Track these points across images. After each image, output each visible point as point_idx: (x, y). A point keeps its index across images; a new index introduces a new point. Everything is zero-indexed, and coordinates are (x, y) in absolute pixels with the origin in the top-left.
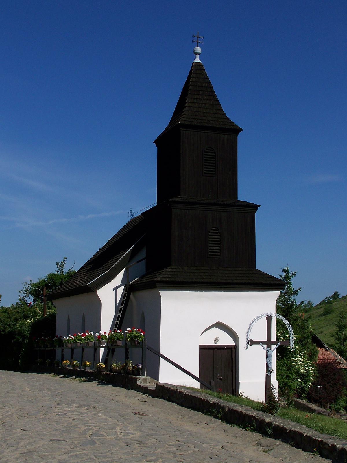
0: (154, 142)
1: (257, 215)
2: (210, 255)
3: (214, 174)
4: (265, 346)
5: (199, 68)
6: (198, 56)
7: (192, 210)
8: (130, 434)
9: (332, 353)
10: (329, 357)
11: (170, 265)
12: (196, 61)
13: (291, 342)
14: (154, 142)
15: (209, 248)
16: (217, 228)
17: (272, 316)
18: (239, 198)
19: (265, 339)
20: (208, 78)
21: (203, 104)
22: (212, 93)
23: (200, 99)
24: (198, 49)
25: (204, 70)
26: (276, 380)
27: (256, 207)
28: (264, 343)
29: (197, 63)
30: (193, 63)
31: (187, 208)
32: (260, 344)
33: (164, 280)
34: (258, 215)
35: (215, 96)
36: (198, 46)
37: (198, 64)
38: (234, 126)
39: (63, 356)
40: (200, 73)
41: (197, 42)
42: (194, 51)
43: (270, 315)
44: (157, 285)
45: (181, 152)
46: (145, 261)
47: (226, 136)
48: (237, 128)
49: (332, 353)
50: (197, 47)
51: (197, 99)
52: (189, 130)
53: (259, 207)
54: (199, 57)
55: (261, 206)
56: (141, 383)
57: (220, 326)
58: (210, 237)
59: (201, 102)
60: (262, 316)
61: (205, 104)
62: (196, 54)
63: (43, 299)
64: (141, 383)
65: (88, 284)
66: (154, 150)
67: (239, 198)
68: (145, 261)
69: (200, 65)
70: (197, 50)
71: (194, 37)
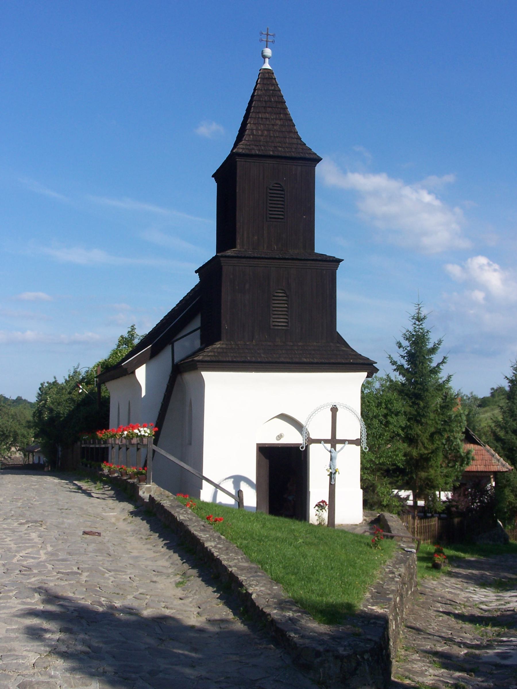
0: (213, 176)
1: (339, 273)
2: (274, 326)
3: (282, 219)
4: (329, 446)
5: (267, 76)
6: (267, 60)
7: (250, 266)
8: (17, 562)
9: (488, 451)
10: (484, 456)
11: (219, 339)
12: (264, 67)
13: (363, 441)
14: (213, 176)
15: (273, 317)
16: (284, 291)
17: (338, 406)
18: (316, 251)
19: (329, 437)
20: (280, 91)
21: (271, 126)
22: (283, 110)
23: (266, 119)
24: (268, 52)
25: (275, 79)
26: (361, 488)
27: (339, 261)
28: (326, 441)
29: (265, 70)
30: (260, 70)
31: (242, 265)
32: (321, 443)
33: (208, 359)
34: (340, 273)
35: (287, 114)
36: (268, 47)
37: (266, 71)
38: (310, 153)
39: (349, 444)
40: (269, 83)
41: (267, 41)
42: (262, 53)
43: (335, 406)
44: (198, 366)
45: (237, 191)
46: (199, 331)
47: (299, 168)
48: (315, 157)
49: (488, 451)
50: (267, 47)
51: (262, 118)
52: (248, 160)
53: (341, 261)
54: (269, 61)
55: (343, 260)
56: (144, 493)
57: (284, 417)
58: (274, 302)
59: (268, 123)
60: (325, 407)
61: (273, 125)
62: (264, 57)
63: (96, 380)
64: (144, 493)
65: (123, 364)
66: (213, 185)
67: (316, 251)
68: (199, 331)
69: (268, 73)
70: (267, 52)
71: (262, 34)
